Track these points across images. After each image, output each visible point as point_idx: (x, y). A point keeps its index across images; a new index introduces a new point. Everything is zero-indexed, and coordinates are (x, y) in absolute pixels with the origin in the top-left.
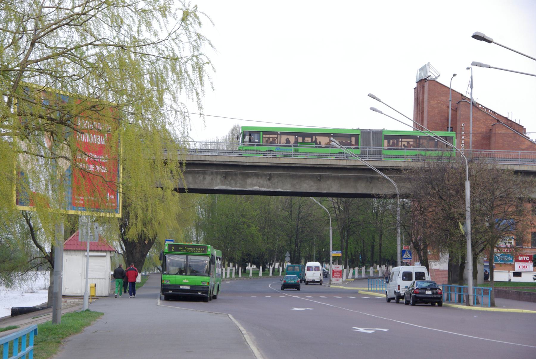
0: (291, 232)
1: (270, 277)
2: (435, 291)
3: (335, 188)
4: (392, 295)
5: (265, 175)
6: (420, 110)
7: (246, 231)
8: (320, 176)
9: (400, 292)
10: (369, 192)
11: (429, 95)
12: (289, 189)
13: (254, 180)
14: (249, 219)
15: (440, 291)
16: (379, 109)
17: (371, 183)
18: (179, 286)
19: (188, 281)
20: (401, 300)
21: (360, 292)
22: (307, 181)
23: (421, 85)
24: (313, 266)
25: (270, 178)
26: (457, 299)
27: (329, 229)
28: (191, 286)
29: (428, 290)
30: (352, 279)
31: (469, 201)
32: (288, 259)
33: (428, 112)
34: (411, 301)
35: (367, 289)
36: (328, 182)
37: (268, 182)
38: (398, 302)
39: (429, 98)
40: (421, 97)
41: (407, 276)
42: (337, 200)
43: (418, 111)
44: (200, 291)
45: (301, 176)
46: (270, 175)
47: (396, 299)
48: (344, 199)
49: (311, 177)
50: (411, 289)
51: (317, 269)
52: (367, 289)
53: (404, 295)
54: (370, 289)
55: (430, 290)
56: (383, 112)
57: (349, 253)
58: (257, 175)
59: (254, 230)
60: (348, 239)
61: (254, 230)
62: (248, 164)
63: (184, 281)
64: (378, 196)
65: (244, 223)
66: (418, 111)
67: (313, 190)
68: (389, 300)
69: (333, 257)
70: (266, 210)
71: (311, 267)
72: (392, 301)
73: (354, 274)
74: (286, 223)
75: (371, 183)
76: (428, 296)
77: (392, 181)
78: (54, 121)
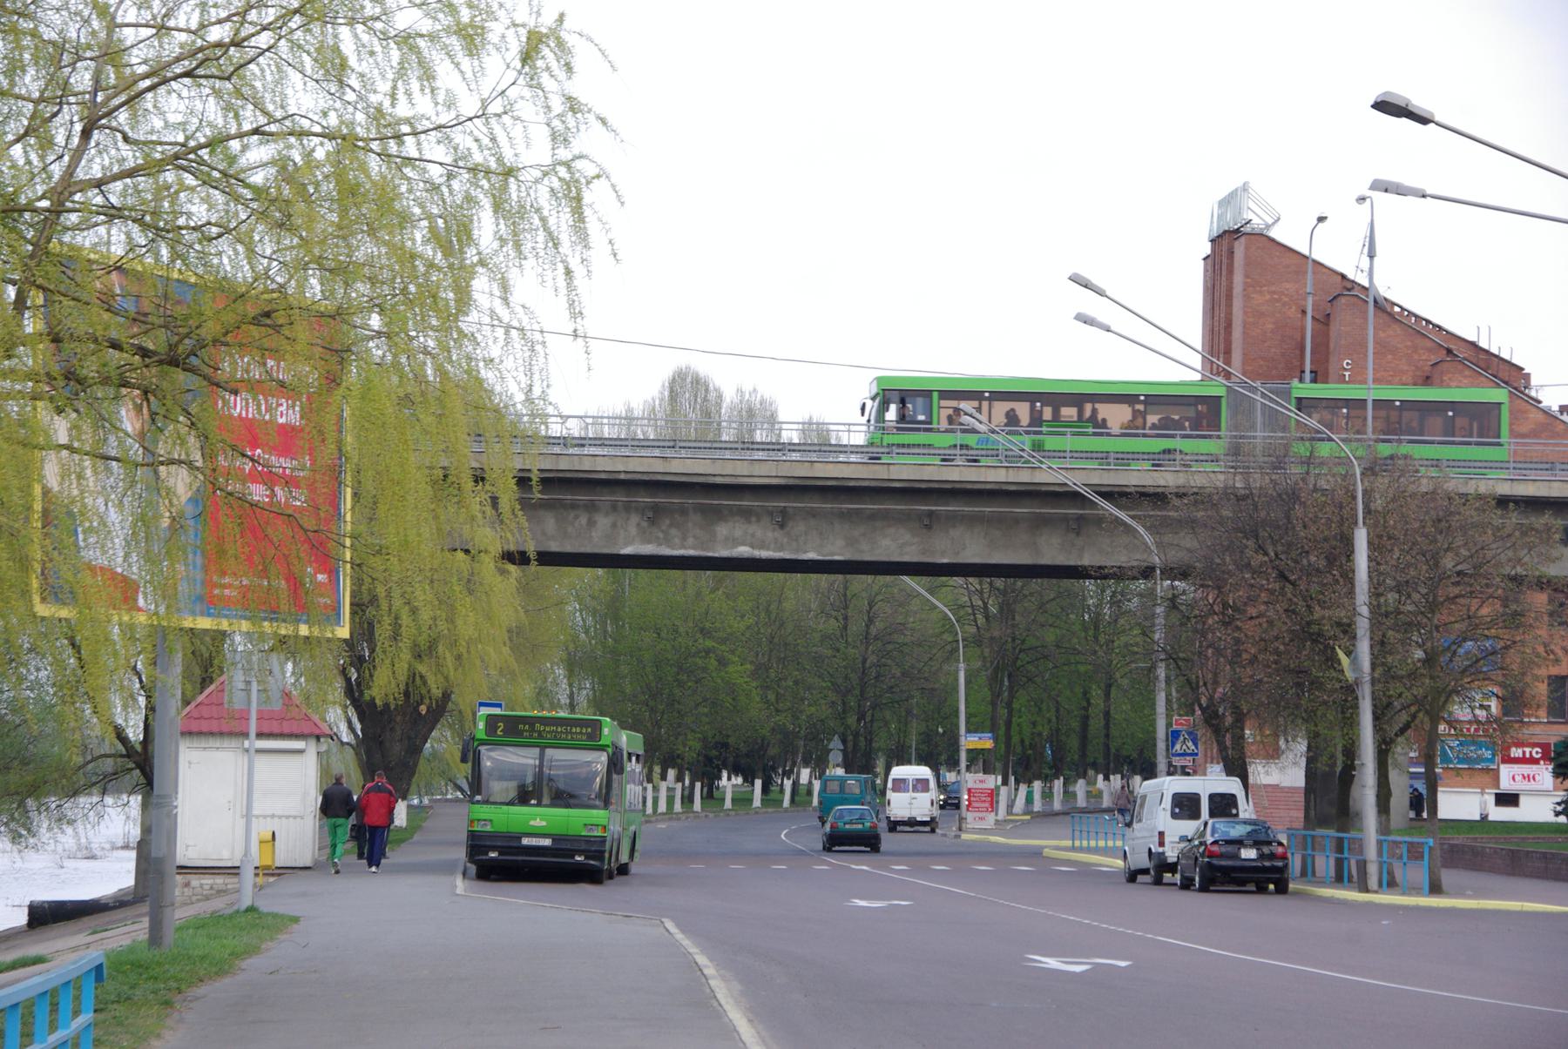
0: (846, 678)
1: (786, 810)
2: (1266, 850)
3: (974, 550)
4: (1144, 862)
5: (771, 513)
6: (1222, 320)
7: (714, 674)
8: (931, 514)
9: (1163, 853)
10: (1072, 561)
11: (1247, 276)
12: (839, 555)
13: (737, 528)
14: (723, 641)
15: (1280, 850)
16: (1101, 318)
17: (1078, 534)
18: (519, 838)
19: (544, 823)
20: (1167, 876)
21: (1047, 852)
22: (892, 530)
23: (1225, 248)
24: (911, 778)
25: (783, 520)
26: (1332, 873)
27: (957, 671)
28: (556, 838)
29: (1245, 846)
30: (1025, 813)
31: (1366, 587)
32: (836, 756)
33: (1244, 327)
34: (1197, 879)
35: (1069, 843)
36: (956, 533)
37: (778, 534)
38: (1158, 881)
39: (1246, 286)
40: (1224, 284)
41: (1185, 806)
42: (981, 584)
43: (1216, 324)
44: (580, 852)
45: (873, 517)
46: (784, 511)
47: (1152, 872)
48: (999, 583)
49: (903, 519)
50: (1196, 843)
51: (922, 785)
52: (1069, 843)
53: (1175, 860)
54: (1077, 843)
55: (1251, 847)
56: (1112, 328)
57: (1015, 739)
58: (746, 514)
59: (739, 672)
60: (1012, 696)
61: (739, 672)
62: (719, 480)
63: (532, 823)
64: (1100, 574)
65: (708, 651)
66: (1216, 324)
67: (911, 555)
68: (1133, 876)
69: (969, 751)
70: (773, 617)
71: (904, 781)
72: (1140, 878)
73: (1029, 800)
74: (830, 652)
75: (1078, 534)
76: (1247, 864)
77: (1141, 530)
78: (149, 357)
